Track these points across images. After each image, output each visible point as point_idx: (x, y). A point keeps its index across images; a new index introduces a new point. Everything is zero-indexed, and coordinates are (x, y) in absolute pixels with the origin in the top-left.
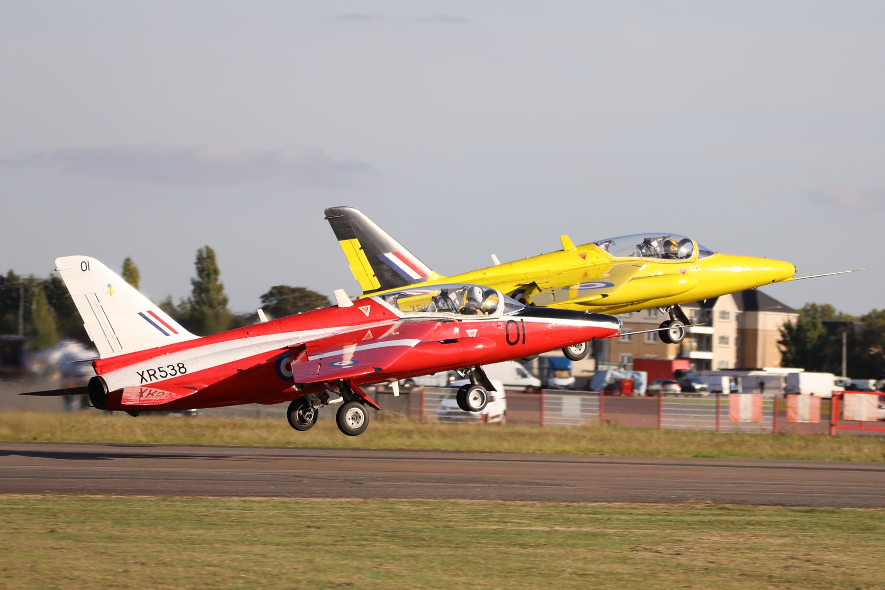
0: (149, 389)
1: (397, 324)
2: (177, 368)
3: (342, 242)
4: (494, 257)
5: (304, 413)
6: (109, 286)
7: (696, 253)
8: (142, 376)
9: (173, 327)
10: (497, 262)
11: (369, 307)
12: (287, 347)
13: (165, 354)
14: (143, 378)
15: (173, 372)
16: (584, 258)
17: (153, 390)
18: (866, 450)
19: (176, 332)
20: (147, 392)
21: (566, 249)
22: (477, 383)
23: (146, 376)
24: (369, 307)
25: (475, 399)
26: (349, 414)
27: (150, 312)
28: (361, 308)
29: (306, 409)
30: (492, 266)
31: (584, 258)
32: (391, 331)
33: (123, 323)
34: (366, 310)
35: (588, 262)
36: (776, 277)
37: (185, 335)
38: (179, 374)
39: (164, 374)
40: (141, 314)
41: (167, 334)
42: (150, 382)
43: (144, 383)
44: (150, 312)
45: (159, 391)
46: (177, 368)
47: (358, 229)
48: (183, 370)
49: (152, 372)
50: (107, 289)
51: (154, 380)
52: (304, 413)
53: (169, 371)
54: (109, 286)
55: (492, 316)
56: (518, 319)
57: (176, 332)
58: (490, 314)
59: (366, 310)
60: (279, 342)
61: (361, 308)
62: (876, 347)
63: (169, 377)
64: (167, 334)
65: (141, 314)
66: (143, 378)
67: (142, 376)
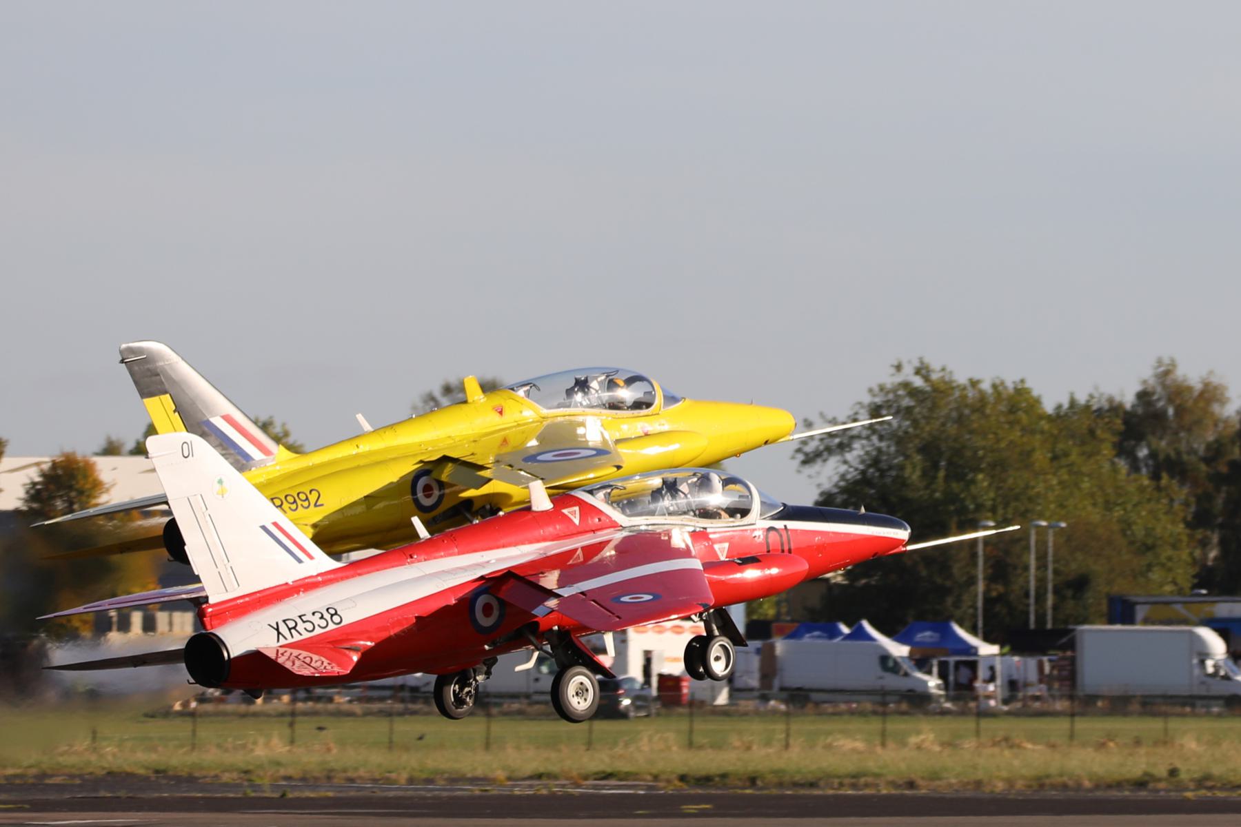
0: (290, 651)
1: (619, 536)
2: (327, 616)
3: (147, 401)
4: (360, 417)
5: (461, 689)
6: (220, 482)
7: (659, 400)
8: (277, 629)
9: (306, 547)
10: (367, 427)
11: (577, 508)
12: (482, 578)
13: (298, 593)
14: (279, 633)
15: (323, 623)
16: (501, 413)
17: (296, 652)
18: (644, 745)
19: (311, 557)
20: (287, 655)
21: (470, 400)
22: (716, 633)
23: (283, 629)
24: (577, 508)
25: (717, 659)
26: (571, 689)
27: (275, 524)
28: (565, 511)
29: (464, 683)
30: (359, 435)
31: (501, 413)
32: (609, 552)
33: (249, 545)
34: (573, 514)
35: (509, 419)
36: (769, 436)
37: (323, 562)
38: (332, 626)
39: (310, 627)
40: (264, 528)
41: (300, 561)
42: (290, 640)
43: (283, 641)
44: (275, 524)
45: (304, 654)
46: (327, 616)
47: (174, 382)
48: (336, 619)
49: (291, 624)
50: (218, 486)
51: (297, 637)
52: (461, 689)
53: (316, 619)
54: (220, 482)
55: (746, 520)
56: (779, 524)
57: (311, 557)
58: (742, 516)
59: (573, 514)
60: (464, 569)
61: (565, 511)
62: (1216, 559)
63: (318, 631)
64: (300, 561)
65: (264, 528)
66: (279, 633)
67: (277, 629)
